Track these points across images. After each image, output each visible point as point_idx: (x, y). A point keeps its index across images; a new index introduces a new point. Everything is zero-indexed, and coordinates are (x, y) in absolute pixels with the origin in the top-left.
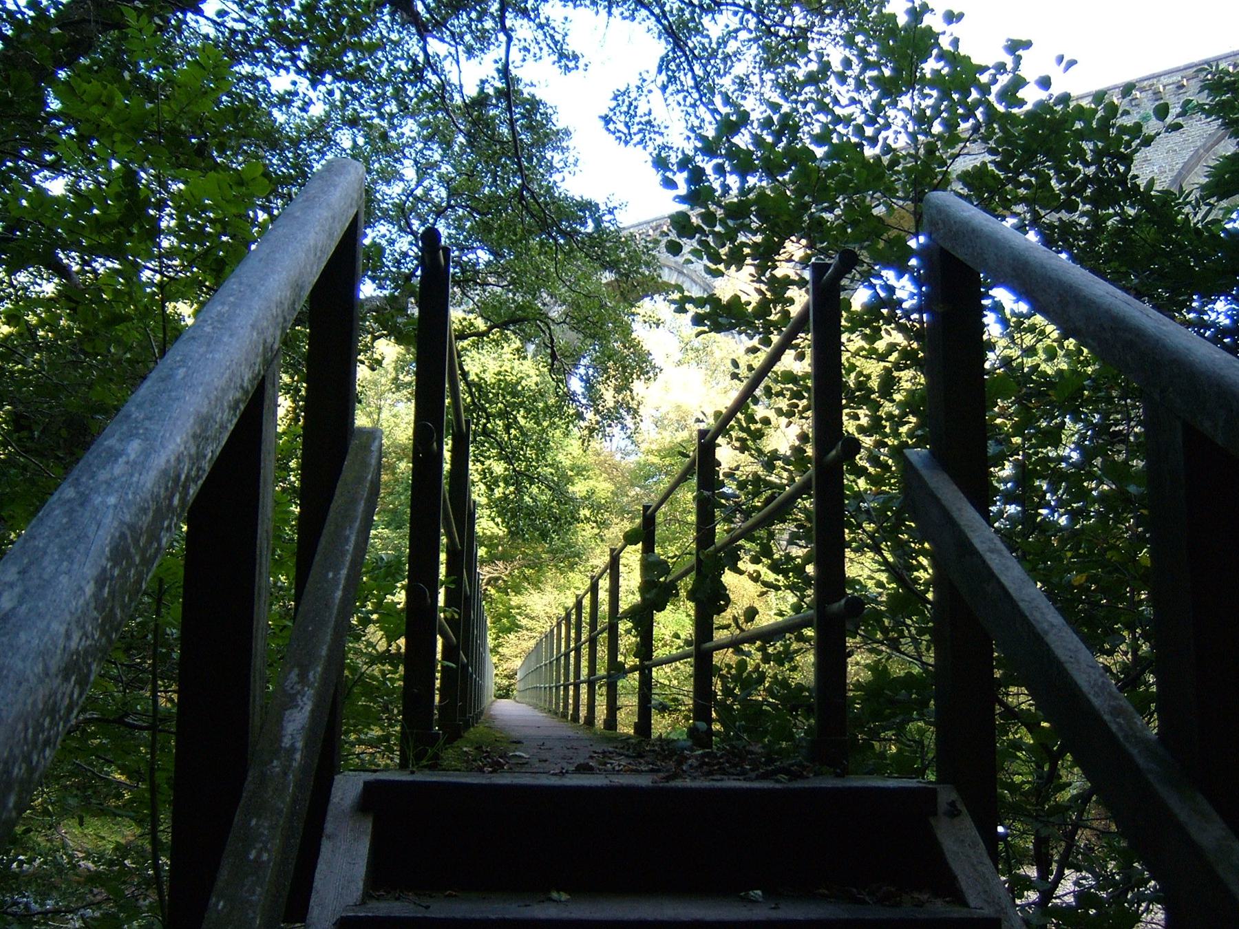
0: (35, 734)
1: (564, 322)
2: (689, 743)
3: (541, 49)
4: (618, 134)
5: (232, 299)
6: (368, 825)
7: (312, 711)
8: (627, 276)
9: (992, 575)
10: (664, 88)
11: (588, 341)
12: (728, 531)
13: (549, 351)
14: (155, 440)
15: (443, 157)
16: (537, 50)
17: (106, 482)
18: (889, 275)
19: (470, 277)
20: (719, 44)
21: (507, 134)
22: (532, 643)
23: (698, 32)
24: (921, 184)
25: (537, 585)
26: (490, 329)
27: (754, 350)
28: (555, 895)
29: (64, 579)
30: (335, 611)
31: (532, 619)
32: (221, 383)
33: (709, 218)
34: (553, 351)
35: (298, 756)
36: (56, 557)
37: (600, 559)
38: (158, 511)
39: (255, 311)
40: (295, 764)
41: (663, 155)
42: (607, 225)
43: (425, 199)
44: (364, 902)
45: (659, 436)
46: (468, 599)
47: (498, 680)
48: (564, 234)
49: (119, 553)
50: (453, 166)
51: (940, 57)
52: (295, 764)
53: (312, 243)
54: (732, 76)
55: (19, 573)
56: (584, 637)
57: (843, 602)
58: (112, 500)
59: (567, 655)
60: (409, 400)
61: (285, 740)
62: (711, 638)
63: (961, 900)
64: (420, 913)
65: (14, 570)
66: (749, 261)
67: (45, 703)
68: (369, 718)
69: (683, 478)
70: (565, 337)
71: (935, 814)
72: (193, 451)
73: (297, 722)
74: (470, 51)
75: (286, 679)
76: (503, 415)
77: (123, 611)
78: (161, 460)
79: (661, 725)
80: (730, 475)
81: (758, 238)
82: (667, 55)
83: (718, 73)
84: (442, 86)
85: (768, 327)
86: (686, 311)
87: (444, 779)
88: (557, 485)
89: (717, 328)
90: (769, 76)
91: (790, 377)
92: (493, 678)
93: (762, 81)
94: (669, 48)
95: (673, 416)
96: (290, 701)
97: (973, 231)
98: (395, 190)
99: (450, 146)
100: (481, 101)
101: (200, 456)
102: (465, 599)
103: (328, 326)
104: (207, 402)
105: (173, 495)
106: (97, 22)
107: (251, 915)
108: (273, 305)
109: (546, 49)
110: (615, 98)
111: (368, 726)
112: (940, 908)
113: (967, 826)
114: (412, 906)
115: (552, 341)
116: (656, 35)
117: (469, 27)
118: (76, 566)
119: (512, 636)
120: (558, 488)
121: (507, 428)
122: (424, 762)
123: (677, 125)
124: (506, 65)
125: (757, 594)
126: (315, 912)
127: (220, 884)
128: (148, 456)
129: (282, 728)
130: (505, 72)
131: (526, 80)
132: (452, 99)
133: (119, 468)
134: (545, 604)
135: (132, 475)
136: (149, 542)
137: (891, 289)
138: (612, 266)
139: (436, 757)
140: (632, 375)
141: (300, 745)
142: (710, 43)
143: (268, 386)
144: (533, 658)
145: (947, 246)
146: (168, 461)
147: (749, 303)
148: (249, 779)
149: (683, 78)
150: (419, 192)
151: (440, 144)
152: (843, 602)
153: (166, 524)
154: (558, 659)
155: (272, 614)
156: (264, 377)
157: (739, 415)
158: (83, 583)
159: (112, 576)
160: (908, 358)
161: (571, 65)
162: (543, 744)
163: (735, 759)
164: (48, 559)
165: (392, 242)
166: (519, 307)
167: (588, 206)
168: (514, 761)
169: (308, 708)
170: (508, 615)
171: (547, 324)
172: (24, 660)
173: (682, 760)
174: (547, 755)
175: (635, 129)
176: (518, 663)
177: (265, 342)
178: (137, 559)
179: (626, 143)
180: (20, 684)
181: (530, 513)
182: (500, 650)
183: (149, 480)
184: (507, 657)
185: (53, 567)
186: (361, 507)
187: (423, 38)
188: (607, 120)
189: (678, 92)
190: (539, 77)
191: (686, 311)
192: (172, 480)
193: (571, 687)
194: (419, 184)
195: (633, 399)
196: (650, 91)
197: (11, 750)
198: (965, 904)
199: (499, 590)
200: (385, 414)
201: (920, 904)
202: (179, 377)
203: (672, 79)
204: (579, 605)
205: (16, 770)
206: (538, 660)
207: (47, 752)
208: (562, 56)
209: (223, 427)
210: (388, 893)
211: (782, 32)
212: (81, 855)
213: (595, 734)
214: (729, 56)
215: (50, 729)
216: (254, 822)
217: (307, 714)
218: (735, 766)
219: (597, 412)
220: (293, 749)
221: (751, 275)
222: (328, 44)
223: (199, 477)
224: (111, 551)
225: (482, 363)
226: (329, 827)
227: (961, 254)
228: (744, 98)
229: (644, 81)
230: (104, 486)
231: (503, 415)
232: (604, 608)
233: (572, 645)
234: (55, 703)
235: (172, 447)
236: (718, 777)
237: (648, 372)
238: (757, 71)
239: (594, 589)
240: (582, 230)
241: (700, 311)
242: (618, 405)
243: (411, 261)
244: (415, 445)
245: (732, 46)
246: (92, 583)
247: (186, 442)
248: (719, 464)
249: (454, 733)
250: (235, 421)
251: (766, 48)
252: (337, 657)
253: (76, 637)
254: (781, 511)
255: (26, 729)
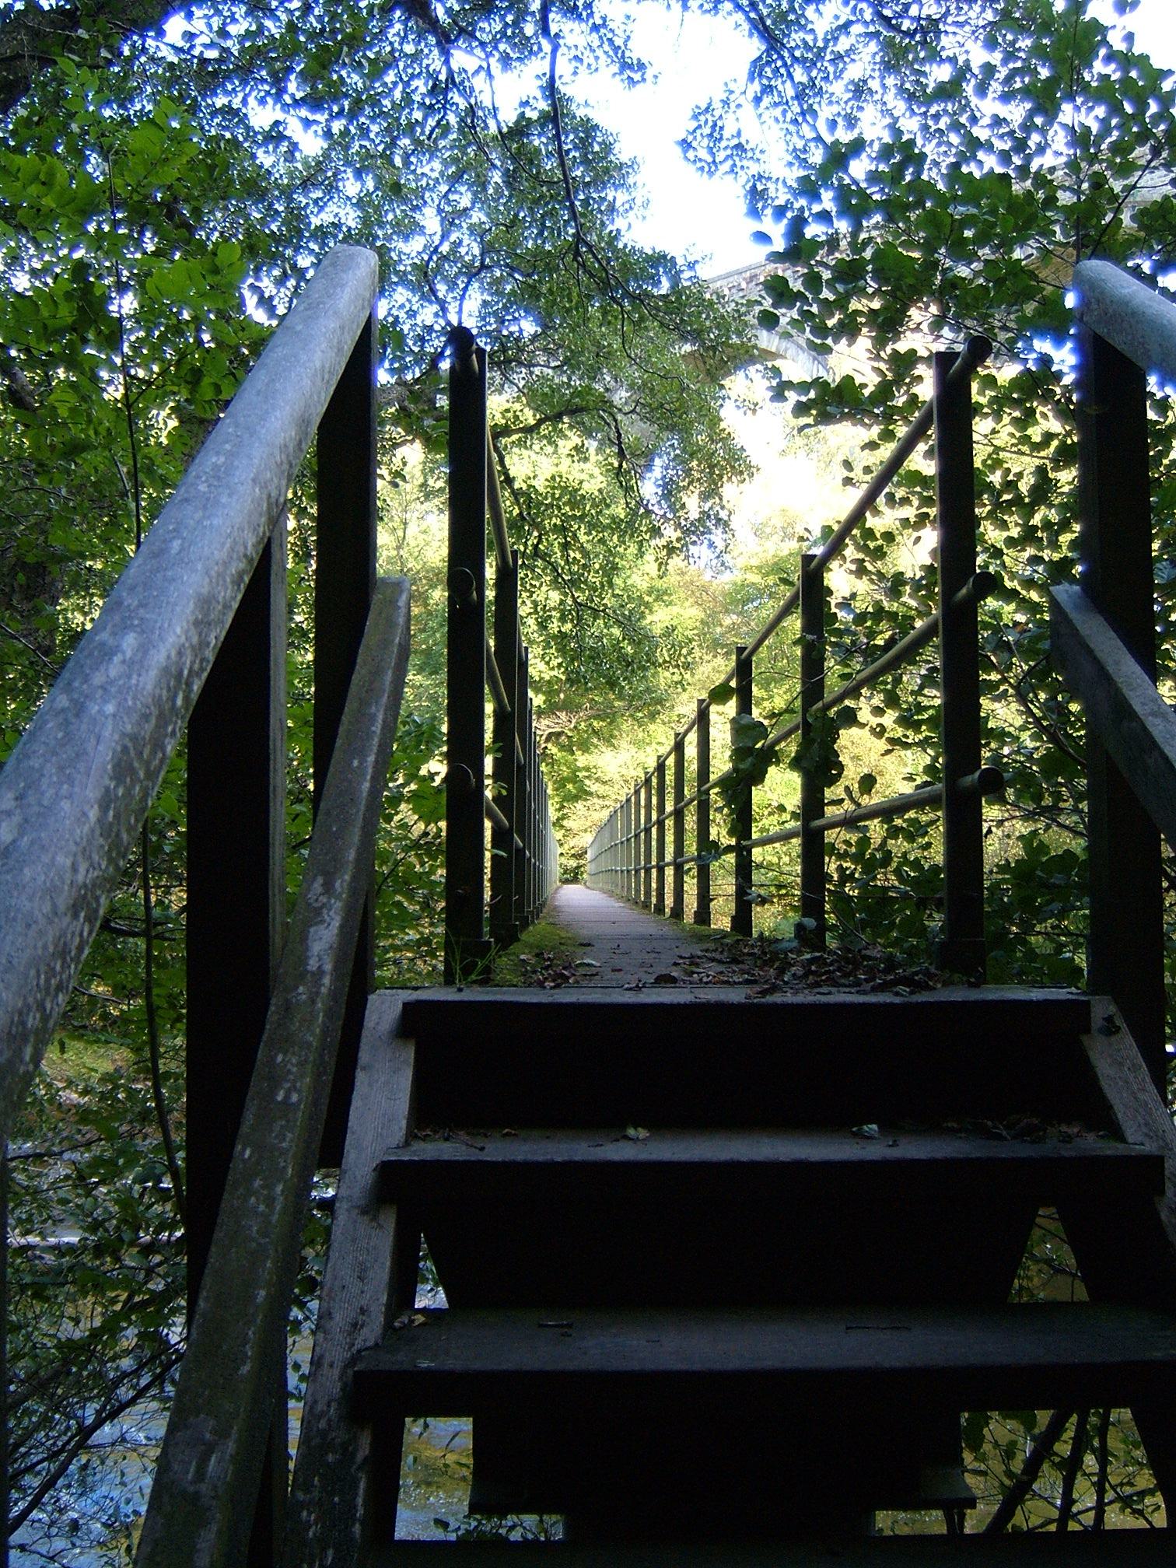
0: (48, 980)
1: (633, 411)
2: (795, 944)
3: (597, 58)
4: (699, 165)
5: (228, 447)
6: (409, 1053)
7: (341, 927)
8: (714, 349)
9: (1154, 745)
10: (758, 100)
11: (665, 435)
12: (844, 677)
13: (615, 449)
14: (153, 633)
15: (473, 203)
16: (592, 60)
17: (102, 687)
18: (1043, 346)
19: (510, 355)
20: (826, 41)
21: (553, 171)
22: (605, 815)
23: (803, 28)
24: (1085, 227)
25: (609, 740)
26: (540, 422)
27: (872, 446)
28: (631, 1132)
29: (66, 805)
30: (363, 808)
31: (605, 783)
32: (220, 555)
33: (813, 281)
34: (621, 451)
35: (327, 981)
36: (55, 779)
37: (690, 710)
38: (161, 716)
39: (256, 461)
40: (324, 990)
41: (760, 187)
42: (686, 284)
43: (453, 256)
44: (407, 1143)
45: (761, 549)
46: (521, 769)
47: (563, 860)
48: (633, 297)
49: (122, 770)
50: (488, 215)
51: (1110, 58)
52: (324, 990)
53: (318, 364)
54: (846, 81)
55: (16, 799)
56: (669, 807)
57: (977, 774)
58: (110, 708)
59: (648, 831)
60: (441, 511)
61: (311, 962)
62: (822, 814)
63: (1116, 1133)
64: (474, 1155)
65: (10, 795)
66: (865, 330)
67: (56, 946)
68: (406, 920)
69: (785, 612)
70: (634, 430)
71: (1087, 1030)
72: (195, 640)
73: (323, 941)
74: (506, 60)
75: (309, 890)
76: (562, 530)
77: (129, 834)
78: (160, 656)
79: (767, 919)
80: (845, 604)
81: (876, 304)
82: (760, 58)
83: (826, 79)
84: (471, 110)
85: (888, 417)
86: (786, 399)
87: (499, 998)
88: (629, 619)
89: (825, 418)
90: (891, 81)
91: (916, 478)
92: (557, 854)
93: (884, 86)
94: (764, 48)
95: (778, 522)
96: (315, 915)
97: (1134, 314)
98: (413, 247)
99: (484, 186)
100: (520, 129)
101: (203, 644)
102: (518, 772)
103: (342, 460)
104: (207, 580)
105: (175, 696)
106: (32, 57)
107: (283, 1164)
108: (277, 452)
109: (603, 57)
110: (695, 117)
111: (402, 929)
112: (1092, 1144)
113: (1127, 1045)
114: (464, 1148)
115: (620, 435)
116: (746, 33)
117: (504, 34)
118: (76, 789)
119: (580, 805)
120: (629, 623)
121: (565, 546)
122: (474, 977)
123: (776, 149)
124: (552, 79)
125: (883, 758)
126: (351, 1154)
127: (245, 1129)
128: (146, 652)
129: (307, 949)
130: (551, 89)
131: (579, 99)
132: (486, 127)
133: (115, 669)
134: (621, 762)
135: (129, 677)
136: (153, 753)
137: (1045, 361)
138: (697, 336)
139: (487, 970)
140: (721, 477)
141: (328, 967)
142: (815, 40)
143: (275, 548)
144: (607, 834)
145: (1102, 331)
146: (169, 657)
147: (864, 386)
148: (273, 1008)
149: (780, 88)
150: (445, 248)
151: (470, 186)
152: (977, 774)
153: (170, 729)
154: (637, 836)
155: (286, 818)
156: (269, 539)
157: (854, 532)
158: (86, 808)
159: (116, 795)
160: (1065, 455)
161: (637, 77)
162: (619, 945)
163: (851, 963)
164: (45, 781)
165: (412, 314)
166: (576, 394)
167: (660, 260)
168: (582, 971)
169: (336, 923)
170: (574, 779)
171: (611, 414)
172: (31, 899)
173: (786, 966)
174: (618, 961)
175: (721, 156)
176: (586, 839)
177: (269, 496)
178: (142, 774)
179: (711, 173)
180: (28, 926)
181: (596, 656)
182: (565, 823)
183: (149, 680)
184: (575, 833)
185: (51, 791)
186: (389, 676)
187: (446, 54)
188: (685, 145)
189: (776, 104)
190: (594, 94)
191: (786, 399)
192: (174, 677)
193: (654, 871)
194: (444, 237)
195: (723, 508)
196: (739, 106)
197: (25, 998)
198: (1122, 1139)
199: (562, 748)
200: (412, 530)
201: (1067, 1139)
202: (173, 552)
203: (768, 89)
204: (661, 768)
205: (31, 1020)
206: (612, 837)
207: (61, 996)
208: (625, 66)
209: (226, 606)
210: (435, 1132)
211: (906, 24)
212: (61, 1085)
213: (683, 930)
214: (841, 57)
215: (61, 974)
216: (280, 1058)
217: (336, 931)
218: (846, 975)
219: (678, 526)
220: (320, 972)
221: (869, 350)
222: (320, 62)
223: (202, 669)
224: (113, 767)
225: (530, 466)
226: (364, 1056)
227: (1118, 341)
228: (860, 109)
229: (732, 92)
230: (100, 692)
231: (562, 530)
232: (692, 767)
233: (654, 817)
234: (65, 944)
235: (171, 639)
236: (825, 989)
237: (741, 473)
238: (877, 74)
239: (679, 747)
240: (655, 292)
241: (804, 399)
242: (705, 515)
243: (438, 337)
244: (450, 567)
245: (843, 44)
246: (96, 806)
247: (187, 631)
248: (830, 592)
249: (508, 936)
250: (239, 597)
251: (888, 45)
252: (368, 851)
253: (83, 868)
254: (909, 655)
255: (39, 976)
